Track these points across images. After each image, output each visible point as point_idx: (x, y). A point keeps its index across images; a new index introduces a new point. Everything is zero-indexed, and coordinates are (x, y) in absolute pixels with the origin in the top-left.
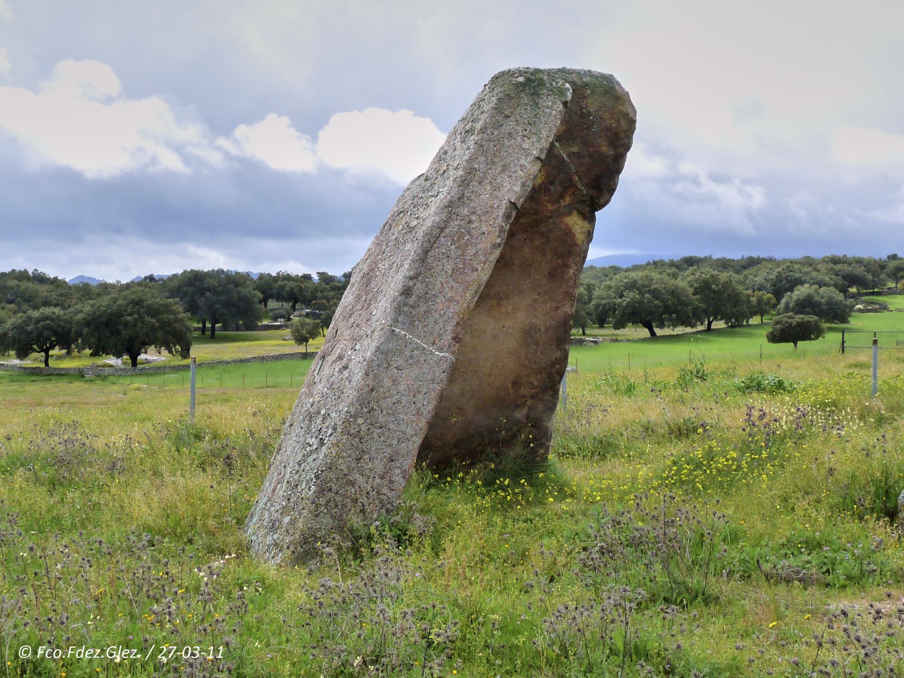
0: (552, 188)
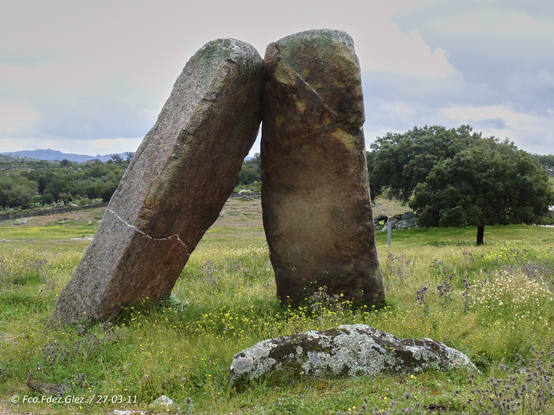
0: (313, 113)
